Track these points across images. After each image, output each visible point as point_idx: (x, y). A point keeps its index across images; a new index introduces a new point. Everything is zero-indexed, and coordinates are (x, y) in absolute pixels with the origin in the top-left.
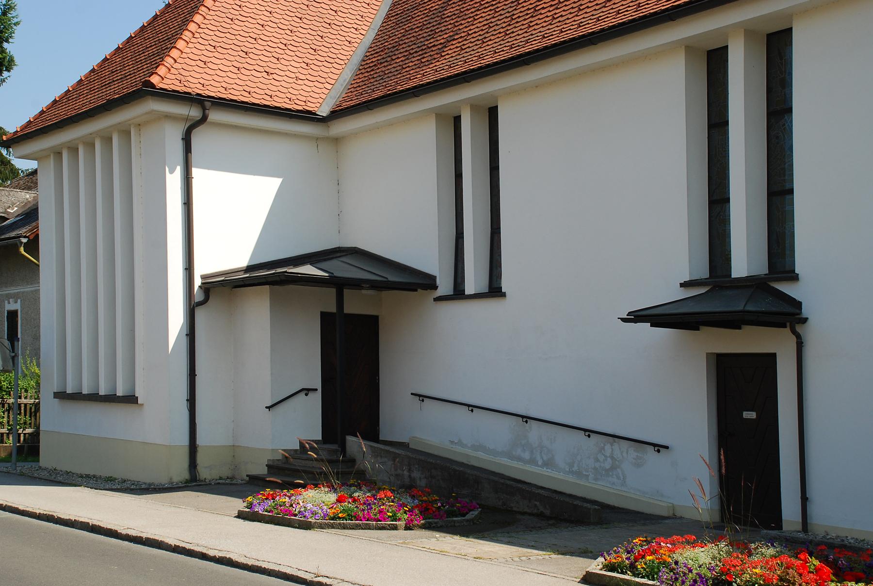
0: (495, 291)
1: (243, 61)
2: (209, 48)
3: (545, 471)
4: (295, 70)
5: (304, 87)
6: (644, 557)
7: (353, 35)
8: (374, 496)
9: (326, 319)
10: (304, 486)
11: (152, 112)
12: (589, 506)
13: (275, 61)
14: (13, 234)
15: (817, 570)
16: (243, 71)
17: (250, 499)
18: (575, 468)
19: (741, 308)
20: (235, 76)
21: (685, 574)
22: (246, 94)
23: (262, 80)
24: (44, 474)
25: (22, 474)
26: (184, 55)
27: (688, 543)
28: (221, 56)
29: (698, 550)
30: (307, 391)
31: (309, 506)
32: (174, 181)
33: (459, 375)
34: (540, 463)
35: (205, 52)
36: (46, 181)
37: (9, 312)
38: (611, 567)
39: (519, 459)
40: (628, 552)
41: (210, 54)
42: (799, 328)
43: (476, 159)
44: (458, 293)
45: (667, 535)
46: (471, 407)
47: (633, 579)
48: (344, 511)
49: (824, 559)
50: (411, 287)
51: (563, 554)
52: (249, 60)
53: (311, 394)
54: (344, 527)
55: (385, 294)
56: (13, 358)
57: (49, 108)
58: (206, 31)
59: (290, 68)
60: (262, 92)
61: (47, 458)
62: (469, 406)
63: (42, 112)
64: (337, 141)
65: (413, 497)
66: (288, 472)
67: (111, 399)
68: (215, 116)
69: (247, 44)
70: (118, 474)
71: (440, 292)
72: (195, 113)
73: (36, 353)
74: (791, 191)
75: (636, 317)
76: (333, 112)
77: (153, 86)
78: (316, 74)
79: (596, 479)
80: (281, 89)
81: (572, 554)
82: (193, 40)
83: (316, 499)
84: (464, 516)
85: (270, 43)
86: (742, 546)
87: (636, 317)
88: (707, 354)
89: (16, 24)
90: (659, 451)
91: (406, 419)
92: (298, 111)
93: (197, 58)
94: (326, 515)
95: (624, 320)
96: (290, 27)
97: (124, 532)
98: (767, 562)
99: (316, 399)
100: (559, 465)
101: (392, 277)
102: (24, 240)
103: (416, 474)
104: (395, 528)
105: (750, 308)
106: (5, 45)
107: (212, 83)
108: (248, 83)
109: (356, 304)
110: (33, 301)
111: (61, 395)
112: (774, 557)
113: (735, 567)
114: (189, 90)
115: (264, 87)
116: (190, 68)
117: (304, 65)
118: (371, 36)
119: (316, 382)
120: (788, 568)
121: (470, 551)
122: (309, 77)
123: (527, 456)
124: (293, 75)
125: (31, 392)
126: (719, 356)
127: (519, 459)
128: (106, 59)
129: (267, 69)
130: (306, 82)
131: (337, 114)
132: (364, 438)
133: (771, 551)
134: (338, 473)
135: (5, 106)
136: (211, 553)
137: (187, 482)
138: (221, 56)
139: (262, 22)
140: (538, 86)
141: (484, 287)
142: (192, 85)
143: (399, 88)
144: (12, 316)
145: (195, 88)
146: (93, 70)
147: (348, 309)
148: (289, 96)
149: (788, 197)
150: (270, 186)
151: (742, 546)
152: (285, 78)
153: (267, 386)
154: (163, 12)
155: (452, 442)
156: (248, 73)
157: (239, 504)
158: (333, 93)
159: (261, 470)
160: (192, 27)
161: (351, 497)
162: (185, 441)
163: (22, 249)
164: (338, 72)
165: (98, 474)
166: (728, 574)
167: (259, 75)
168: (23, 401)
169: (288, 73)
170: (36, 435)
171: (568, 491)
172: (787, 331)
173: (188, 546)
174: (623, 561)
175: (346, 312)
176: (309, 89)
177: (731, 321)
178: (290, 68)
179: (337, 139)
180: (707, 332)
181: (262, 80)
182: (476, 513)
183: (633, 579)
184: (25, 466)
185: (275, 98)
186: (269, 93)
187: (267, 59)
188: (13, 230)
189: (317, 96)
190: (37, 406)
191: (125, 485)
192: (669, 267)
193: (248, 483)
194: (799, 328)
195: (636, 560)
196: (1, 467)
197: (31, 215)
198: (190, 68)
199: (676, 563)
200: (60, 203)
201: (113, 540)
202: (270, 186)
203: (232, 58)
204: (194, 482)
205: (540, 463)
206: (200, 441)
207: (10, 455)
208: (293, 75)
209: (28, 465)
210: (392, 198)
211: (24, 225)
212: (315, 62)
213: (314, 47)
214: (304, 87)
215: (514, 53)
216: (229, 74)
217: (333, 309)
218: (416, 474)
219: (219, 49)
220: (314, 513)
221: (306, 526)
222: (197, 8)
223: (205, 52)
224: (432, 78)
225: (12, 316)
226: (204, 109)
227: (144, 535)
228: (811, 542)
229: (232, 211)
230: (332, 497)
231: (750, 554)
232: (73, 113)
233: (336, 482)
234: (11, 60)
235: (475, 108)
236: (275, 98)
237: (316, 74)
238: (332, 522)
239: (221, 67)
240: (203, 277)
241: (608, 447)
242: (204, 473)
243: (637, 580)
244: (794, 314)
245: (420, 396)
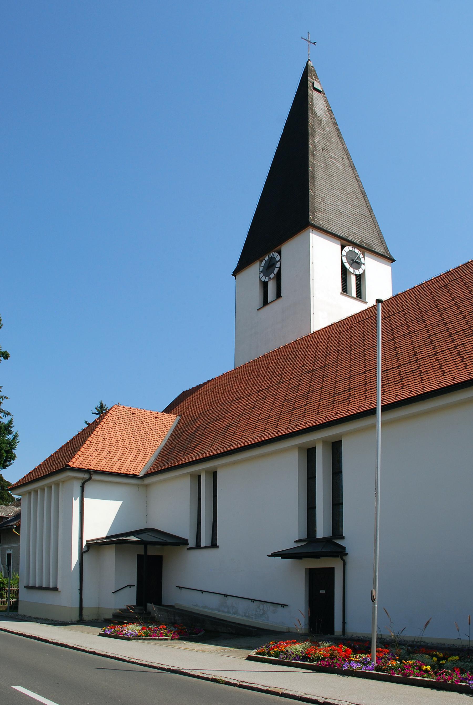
0: (214, 545)
1: (108, 455)
2: (94, 450)
3: (233, 616)
4: (130, 458)
5: (134, 465)
6: (274, 649)
7: (156, 443)
8: (158, 627)
9: (139, 557)
10: (128, 623)
11: (68, 476)
12: (252, 629)
13: (122, 454)
14: (11, 524)
15: (346, 651)
16: (108, 459)
17: (104, 628)
18: (247, 614)
19: (320, 550)
20: (104, 461)
21: (290, 655)
22: (109, 468)
23: (116, 462)
24: (20, 617)
25: (11, 617)
26: (83, 454)
27: (293, 643)
28: (99, 453)
29: (297, 645)
30: (130, 586)
31: (130, 631)
32: (76, 503)
33: (197, 579)
34: (232, 613)
35: (92, 452)
36: (24, 503)
37: (8, 554)
38: (259, 653)
39: (223, 611)
40: (267, 647)
41: (95, 453)
42: (344, 557)
43: (207, 494)
44: (198, 546)
45: (284, 640)
46: (202, 591)
47: (268, 657)
48: (144, 633)
49: (349, 646)
50: (177, 544)
51: (239, 648)
52: (110, 455)
53: (132, 587)
54: (145, 639)
55: (166, 547)
56: (9, 573)
57: (27, 475)
58: (93, 444)
59: (128, 457)
60: (115, 467)
61: (21, 611)
62: (201, 591)
63: (25, 477)
64: (147, 486)
65: (175, 627)
66: (121, 618)
67: (47, 589)
68: (95, 477)
69: (110, 448)
70: (50, 617)
71: (190, 546)
72: (86, 476)
73: (17, 570)
74: (342, 504)
75: (275, 555)
76: (145, 475)
77: (70, 466)
78: (139, 459)
79: (256, 619)
80: (123, 465)
81: (243, 648)
82: (88, 447)
83: (133, 628)
84: (197, 634)
85: (120, 448)
86: (315, 643)
87: (275, 555)
88: (306, 569)
89: (18, 442)
90: (283, 607)
91: (173, 596)
92: (130, 474)
93: (89, 454)
94: (136, 635)
95: (269, 556)
96: (129, 441)
97: (51, 641)
98: (326, 649)
99: (134, 589)
100: (240, 613)
101: (169, 541)
102: (15, 526)
103: (177, 618)
104: (167, 639)
105: (323, 550)
106: (13, 450)
107: (94, 464)
108: (110, 464)
109: (152, 551)
110: (17, 550)
111: (27, 587)
112: (328, 646)
113: (312, 651)
114: (85, 467)
115: (116, 465)
116: (86, 459)
117: (134, 456)
118: (164, 443)
119: (135, 583)
120: (334, 650)
121: (199, 648)
122: (136, 461)
123: (226, 610)
124: (129, 460)
125: (15, 585)
126: (310, 569)
127: (223, 611)
128: (52, 455)
129: (118, 458)
130: (135, 463)
131: (147, 475)
132: (154, 604)
133: (328, 644)
134: (143, 618)
135: (13, 474)
136: (87, 650)
137: (78, 621)
138: (99, 453)
139: (117, 439)
140: (235, 463)
141: (209, 543)
142: (86, 465)
143: (175, 464)
144: (9, 555)
145: (87, 466)
146: (46, 460)
147: (149, 553)
148: (127, 468)
149: (340, 506)
150: (117, 504)
151: (315, 643)
152: (126, 461)
153: (115, 584)
154: (76, 437)
155: (194, 605)
156: (110, 460)
157: (100, 630)
158: (146, 467)
159: (110, 616)
160: (88, 442)
161: (148, 628)
162: (78, 605)
163: (14, 530)
164: (149, 458)
165: (42, 617)
166: (309, 654)
167: (115, 460)
168: (12, 588)
169: (127, 459)
170: (17, 602)
171: (243, 623)
172: (339, 559)
173: (77, 647)
174: (265, 651)
175: (147, 556)
176: (136, 465)
177: (316, 556)
178: (128, 457)
179: (147, 485)
180: (305, 560)
181: (116, 462)
182: (202, 633)
183: (268, 657)
184: (12, 614)
185: (121, 470)
186: (109, 466)
187: (118, 454)
188: (11, 522)
189: (139, 468)
190: (18, 591)
191: (53, 622)
192: (290, 533)
193: (104, 622)
194: (344, 557)
195: (270, 650)
196: (3, 614)
197: (18, 516)
198: (86, 459)
199: (287, 651)
200: (28, 512)
201: (47, 644)
202: (117, 504)
203: (104, 454)
204: (81, 621)
205: (232, 613)
206: (84, 605)
207: (7, 609)
208: (129, 460)
209: (14, 613)
210: (171, 508)
211: (15, 521)
212: (139, 454)
213: (139, 448)
214: (134, 465)
215: (225, 450)
216: (102, 460)
217: (142, 553)
218: (177, 618)
219: (98, 451)
220: (132, 634)
221: (128, 639)
222: (90, 435)
223: (92, 452)
224: (189, 460)
225: (9, 555)
226: (90, 475)
227: (59, 642)
228: (346, 639)
229: (100, 515)
230: (140, 628)
231: (319, 646)
232: (37, 477)
233: (141, 622)
234: (15, 456)
235: (207, 471)
236: (121, 470)
237: (139, 459)
238: (139, 638)
239: (98, 458)
240: (87, 541)
241: (261, 607)
242: (85, 617)
243: (270, 658)
244: (342, 552)
245: (180, 587)
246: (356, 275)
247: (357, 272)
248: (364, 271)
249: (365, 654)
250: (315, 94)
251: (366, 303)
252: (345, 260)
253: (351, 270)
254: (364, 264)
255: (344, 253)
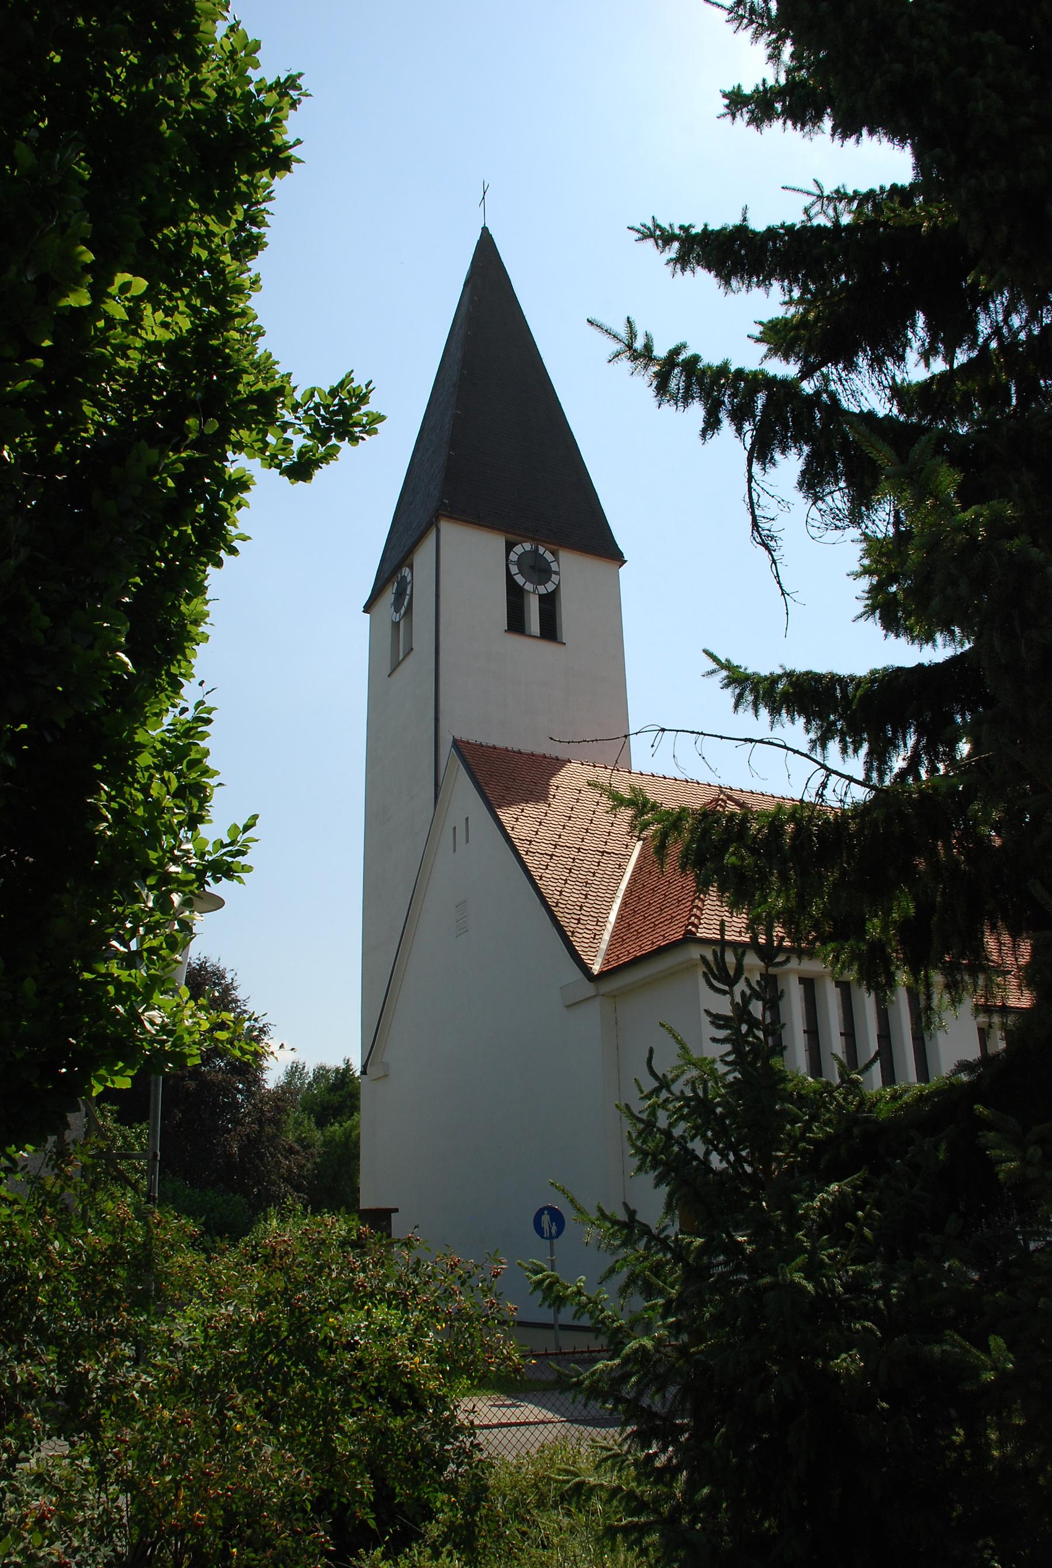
246: (541, 596)
247: (542, 590)
248: (558, 586)
249: (112, 1104)
250: (840, 1055)
251: (342, 417)
252: (514, 569)
253: (529, 587)
254: (557, 573)
255: (513, 557)
